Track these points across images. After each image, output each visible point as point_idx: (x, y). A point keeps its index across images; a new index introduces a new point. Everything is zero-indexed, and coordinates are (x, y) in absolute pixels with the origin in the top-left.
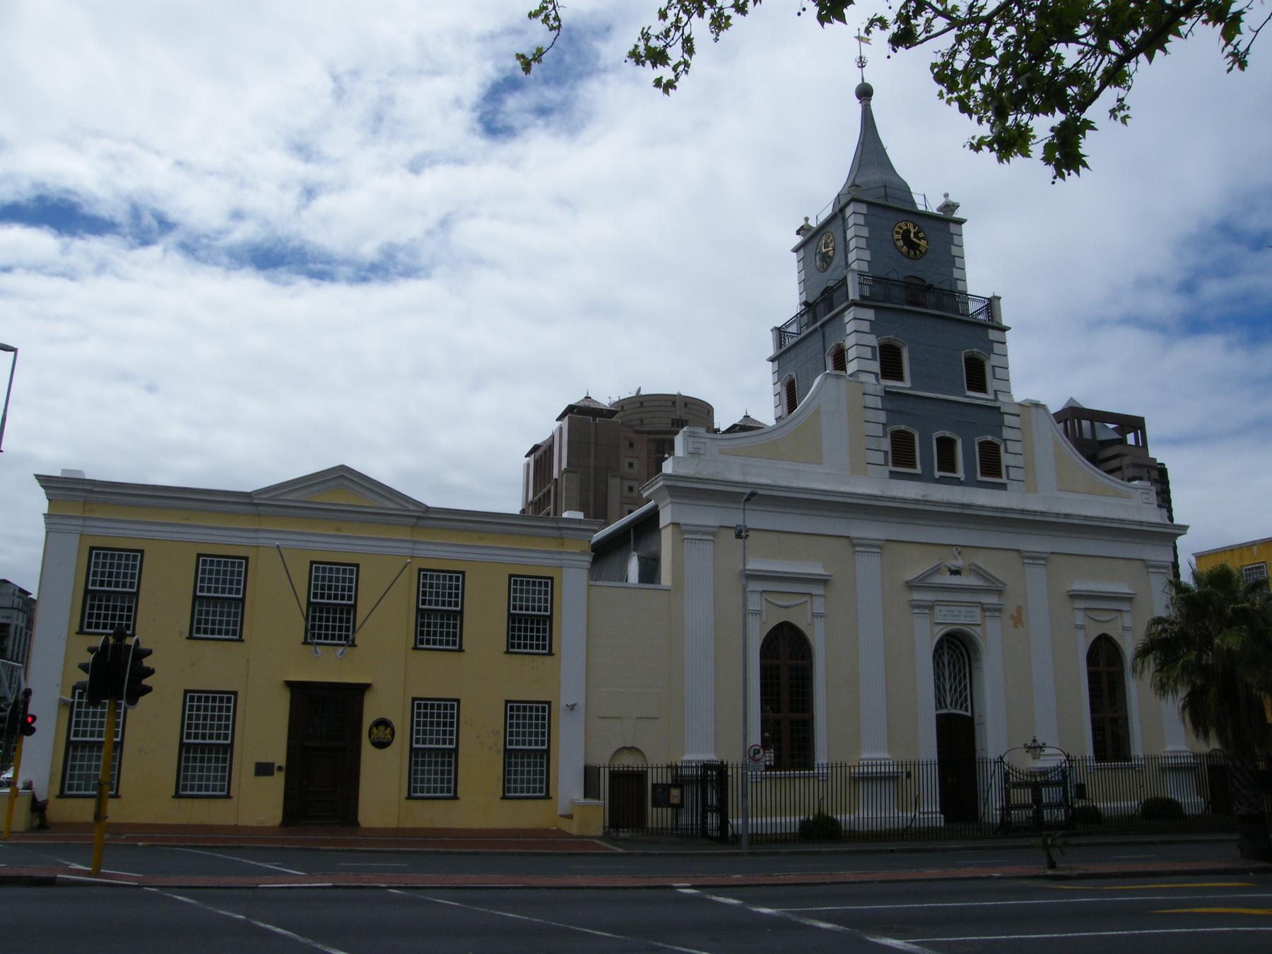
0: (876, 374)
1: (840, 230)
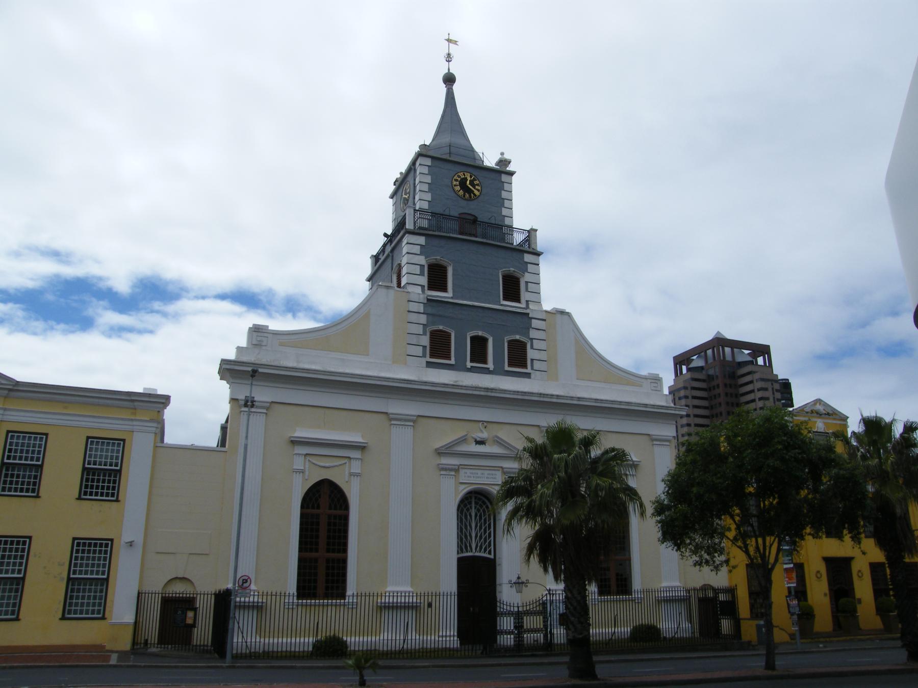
0: (423, 287)
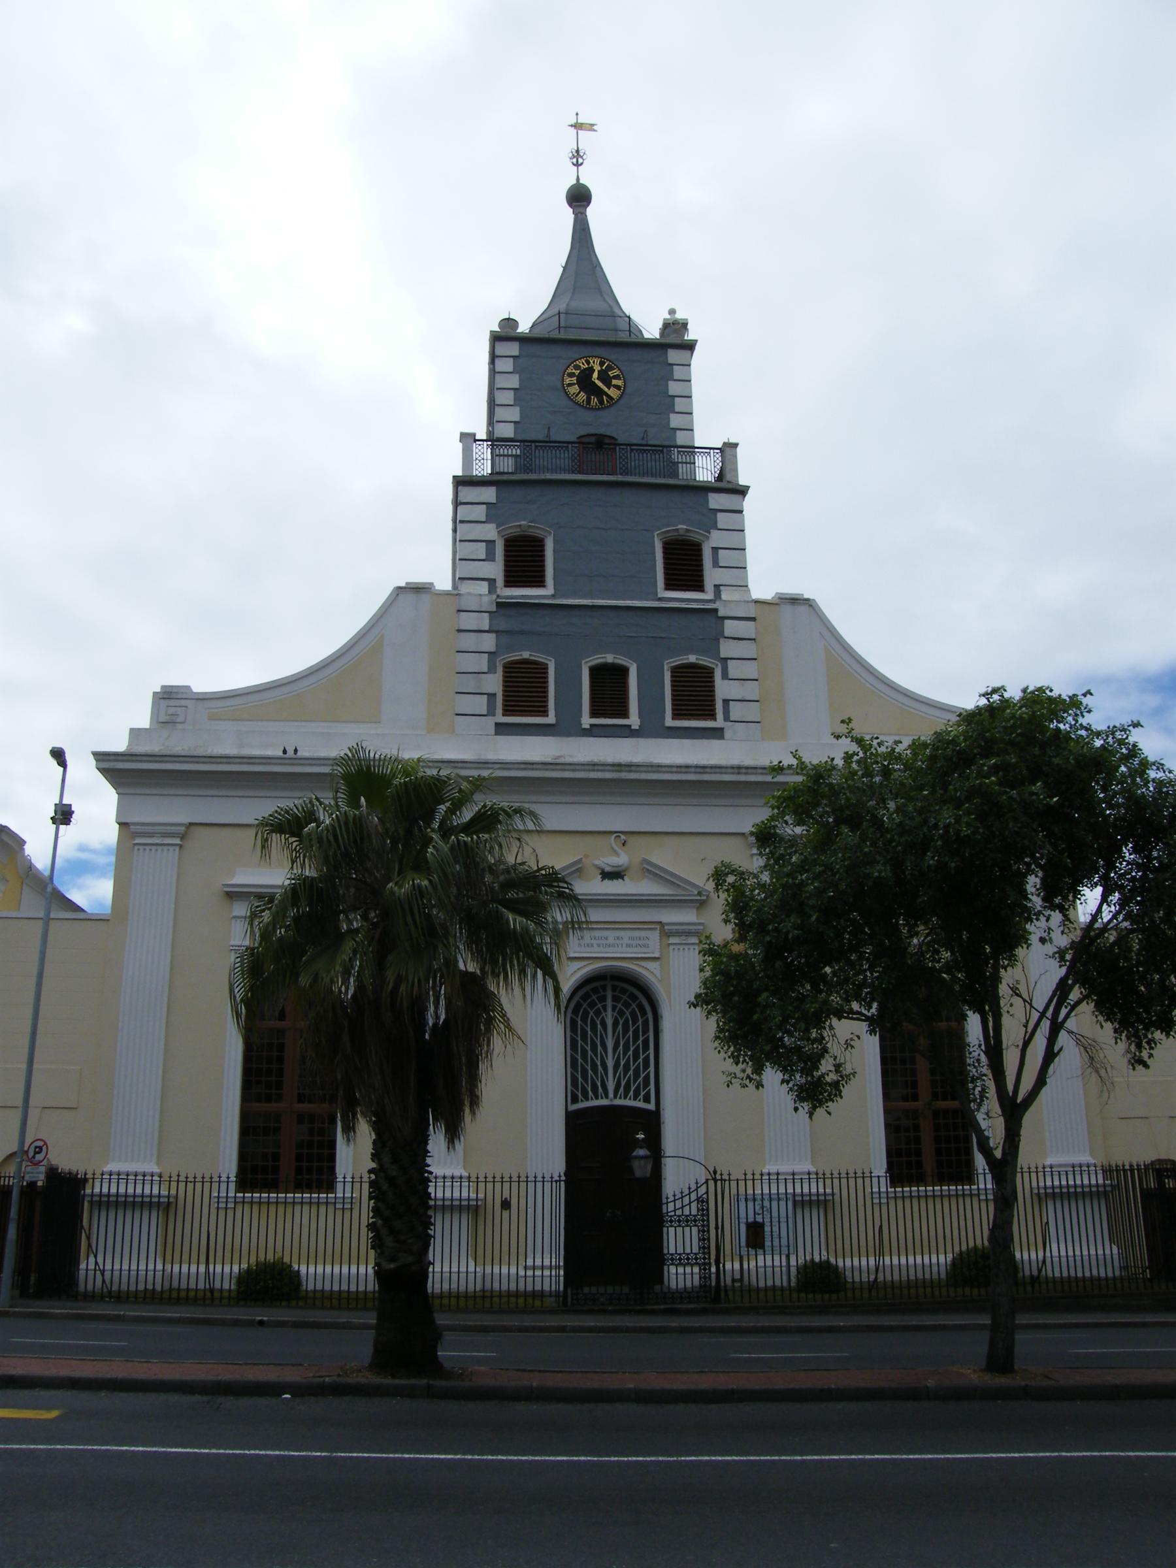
0: (492, 582)
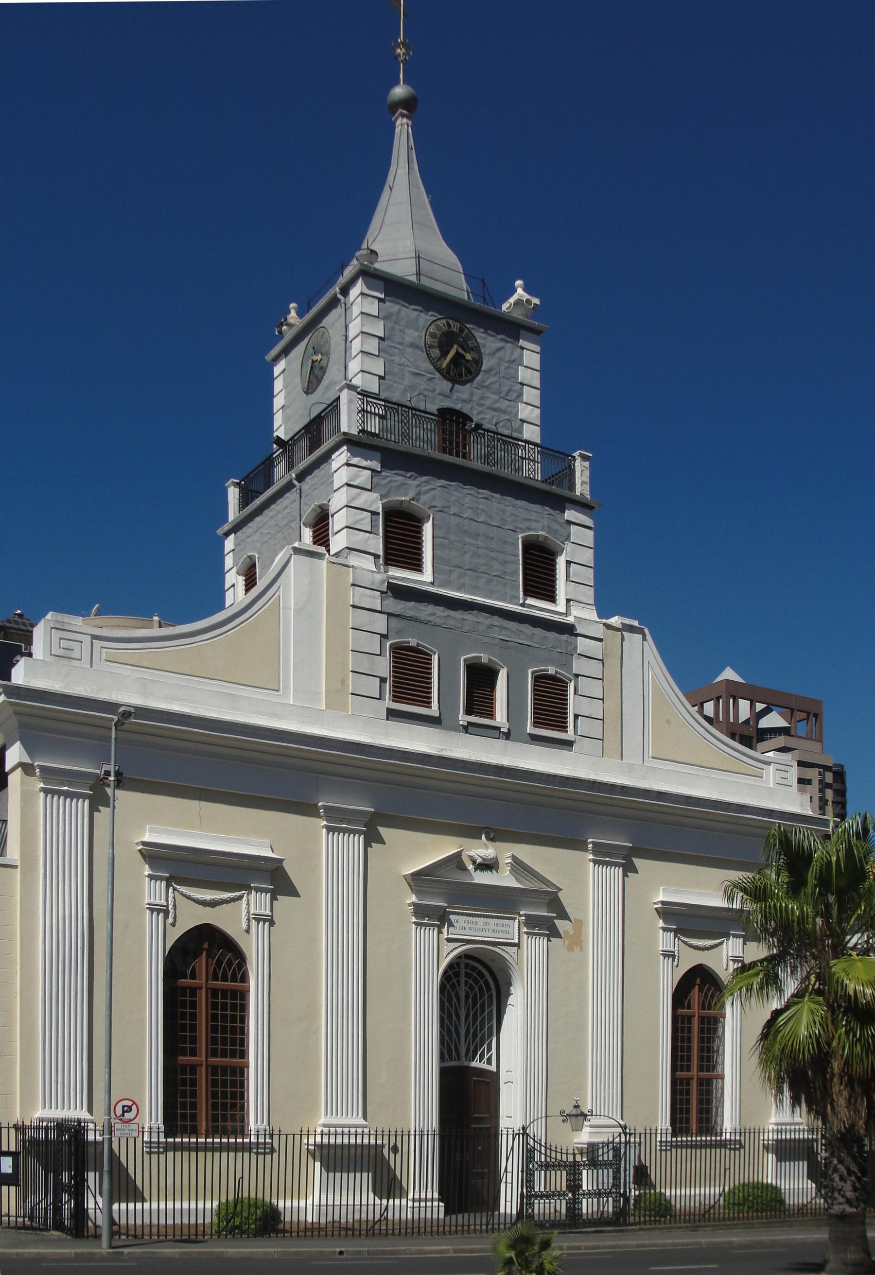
1: (341, 322)
